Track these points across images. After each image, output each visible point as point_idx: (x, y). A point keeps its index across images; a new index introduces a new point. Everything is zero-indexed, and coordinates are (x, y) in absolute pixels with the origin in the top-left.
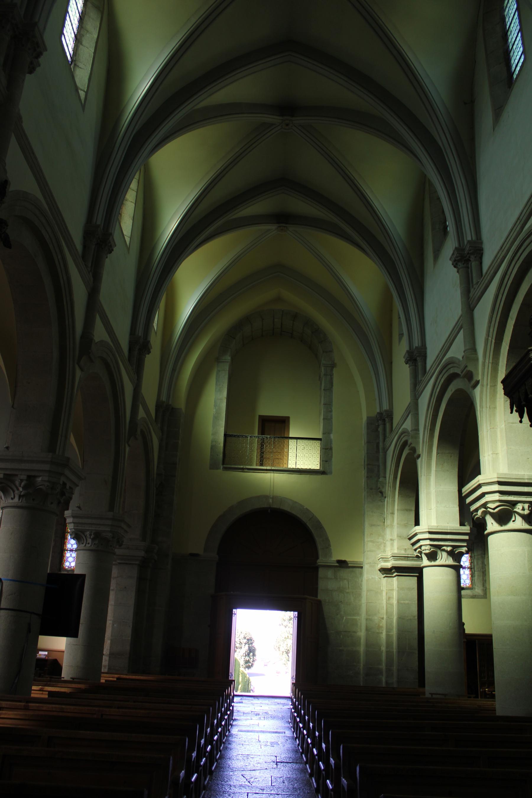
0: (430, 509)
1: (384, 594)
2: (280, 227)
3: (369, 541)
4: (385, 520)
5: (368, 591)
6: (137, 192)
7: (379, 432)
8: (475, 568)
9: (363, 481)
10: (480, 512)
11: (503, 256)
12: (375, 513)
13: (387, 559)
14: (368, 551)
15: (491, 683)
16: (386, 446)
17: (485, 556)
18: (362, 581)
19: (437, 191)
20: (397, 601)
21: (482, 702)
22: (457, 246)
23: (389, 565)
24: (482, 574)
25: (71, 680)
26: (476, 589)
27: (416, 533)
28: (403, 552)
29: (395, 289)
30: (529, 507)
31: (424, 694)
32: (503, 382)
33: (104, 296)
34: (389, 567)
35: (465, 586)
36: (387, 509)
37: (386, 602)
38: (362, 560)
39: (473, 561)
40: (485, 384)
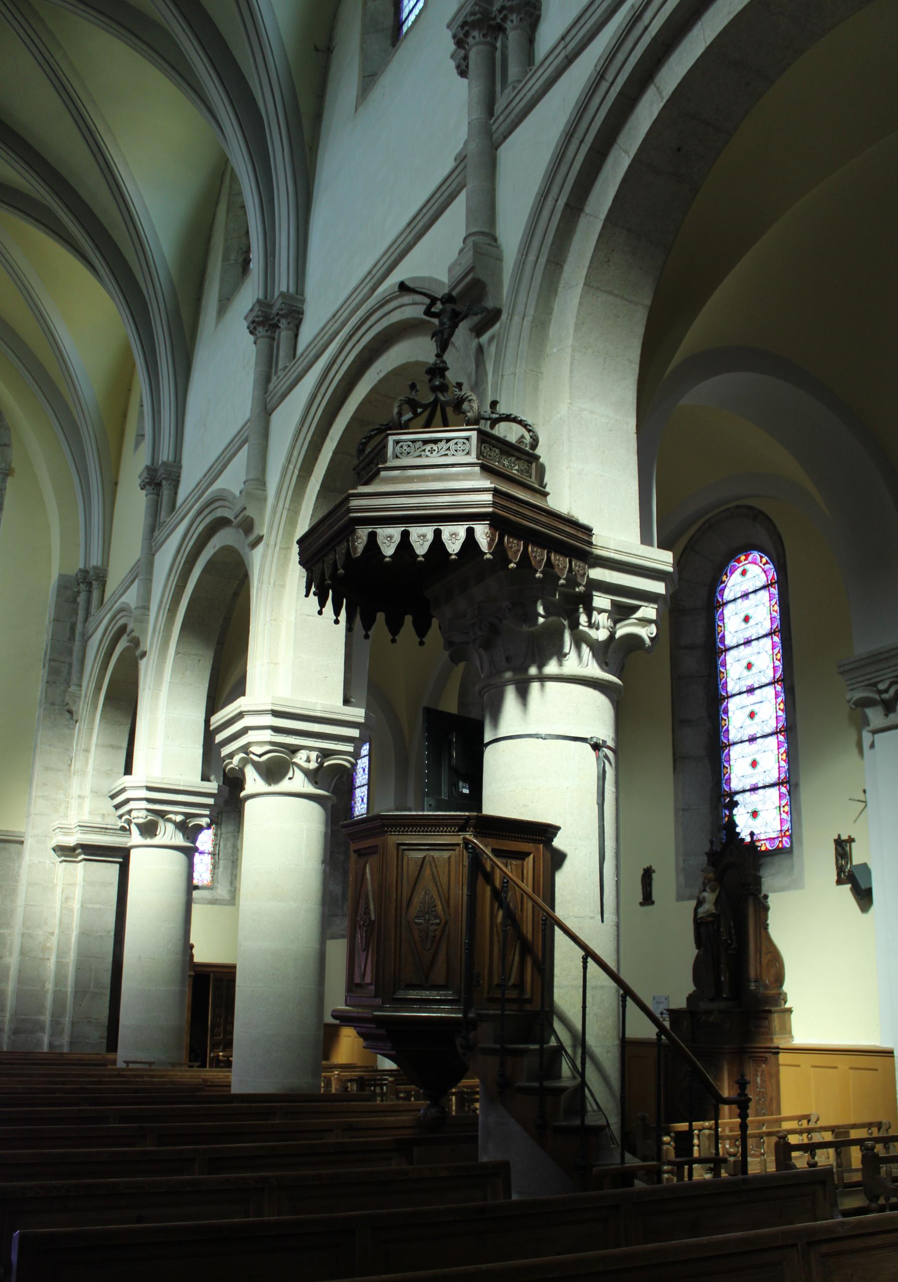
0: (153, 749)
1: (59, 890)
3: (39, 797)
4: (71, 761)
5: (29, 884)
7: (78, 604)
8: (221, 854)
9: (40, 689)
10: (236, 760)
11: (334, 331)
12: (54, 747)
13: (70, 831)
14: (36, 814)
15: (228, 1044)
16: (88, 632)
17: (238, 835)
18: (20, 867)
19: (242, 193)
20: (80, 905)
21: (211, 1074)
22: (261, 297)
23: (71, 841)
24: (230, 864)
26: (219, 890)
27: (125, 788)
28: (99, 819)
29: (141, 353)
30: (318, 757)
31: (114, 1062)
32: (300, 542)
34: (72, 845)
35: (200, 884)
36: (77, 742)
37: (61, 906)
38: (23, 830)
39: (218, 842)
40: (272, 542)
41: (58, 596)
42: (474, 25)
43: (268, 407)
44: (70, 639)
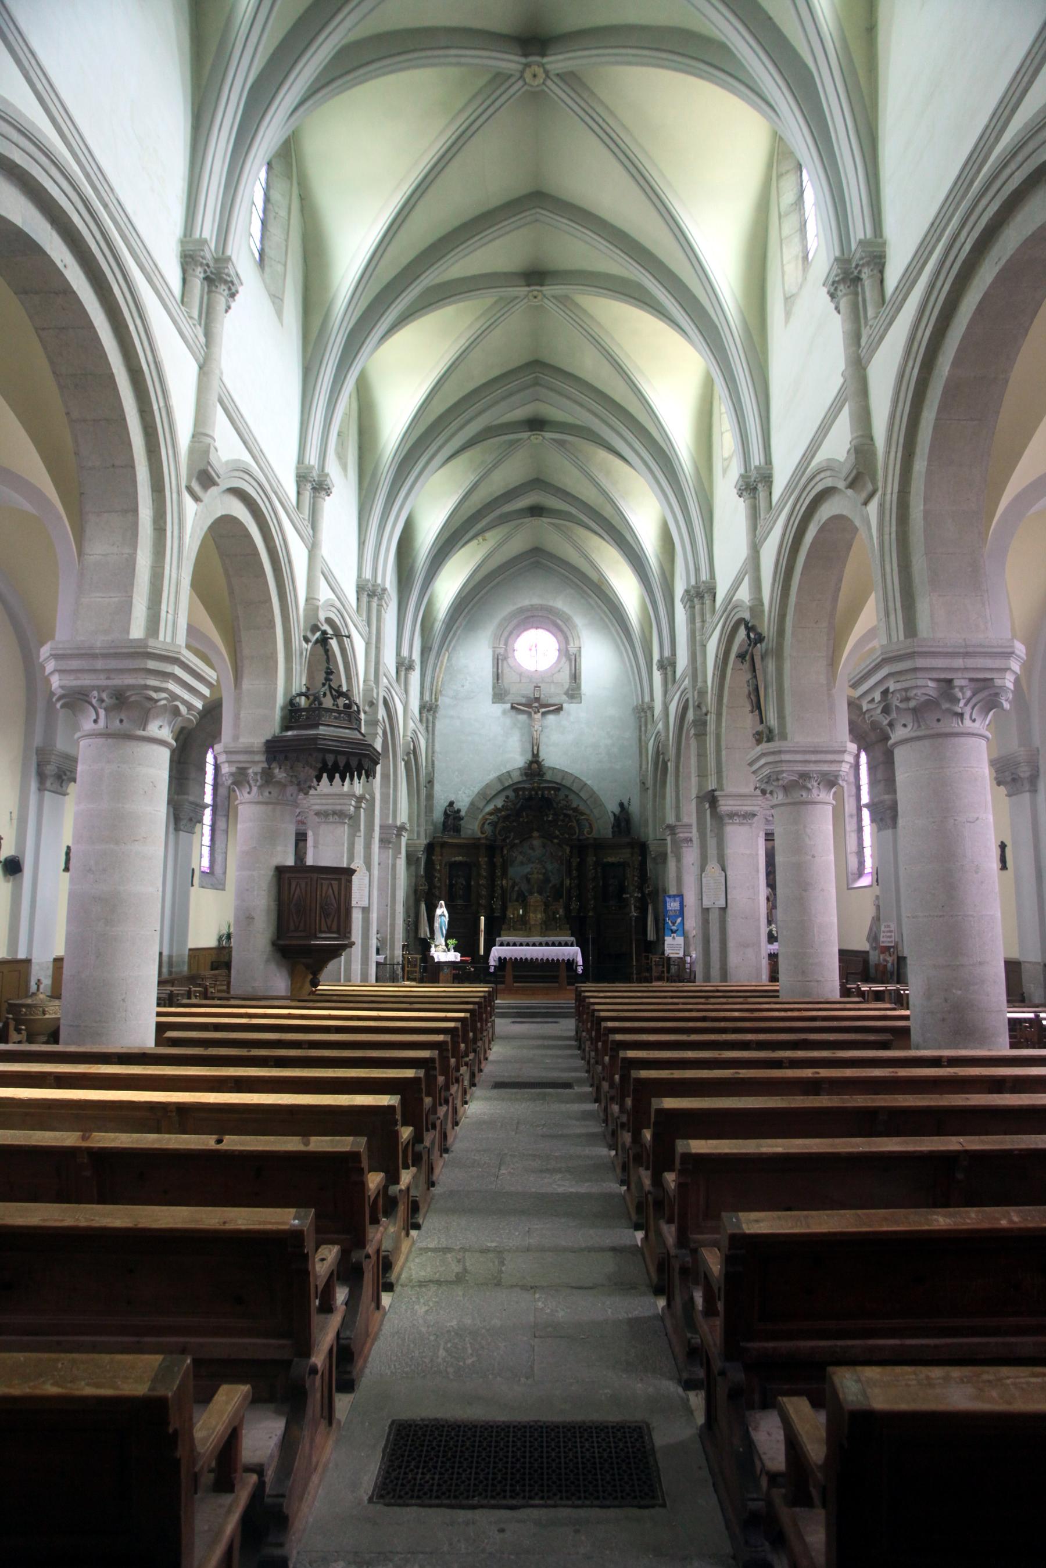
22: (743, 471)
33: (326, 550)
42: (838, 282)
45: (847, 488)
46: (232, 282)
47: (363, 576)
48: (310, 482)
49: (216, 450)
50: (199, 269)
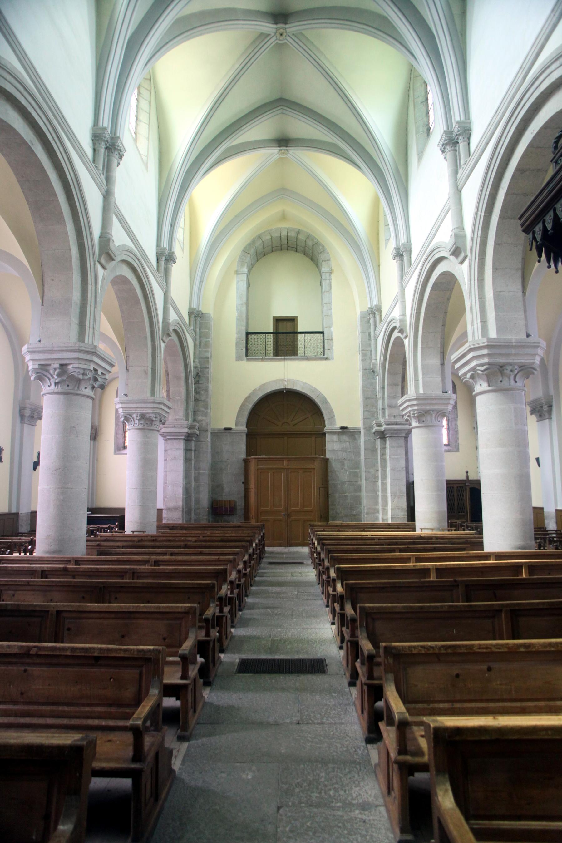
2: (281, 150)
6: (149, 114)
22: (445, 129)
25: (131, 533)
41: (361, 321)
42: (446, 144)
43: (459, 187)
44: (369, 340)
45: (450, 255)
46: (120, 150)
47: (192, 307)
48: (104, 141)
49: (114, 241)
50: (103, 143)
